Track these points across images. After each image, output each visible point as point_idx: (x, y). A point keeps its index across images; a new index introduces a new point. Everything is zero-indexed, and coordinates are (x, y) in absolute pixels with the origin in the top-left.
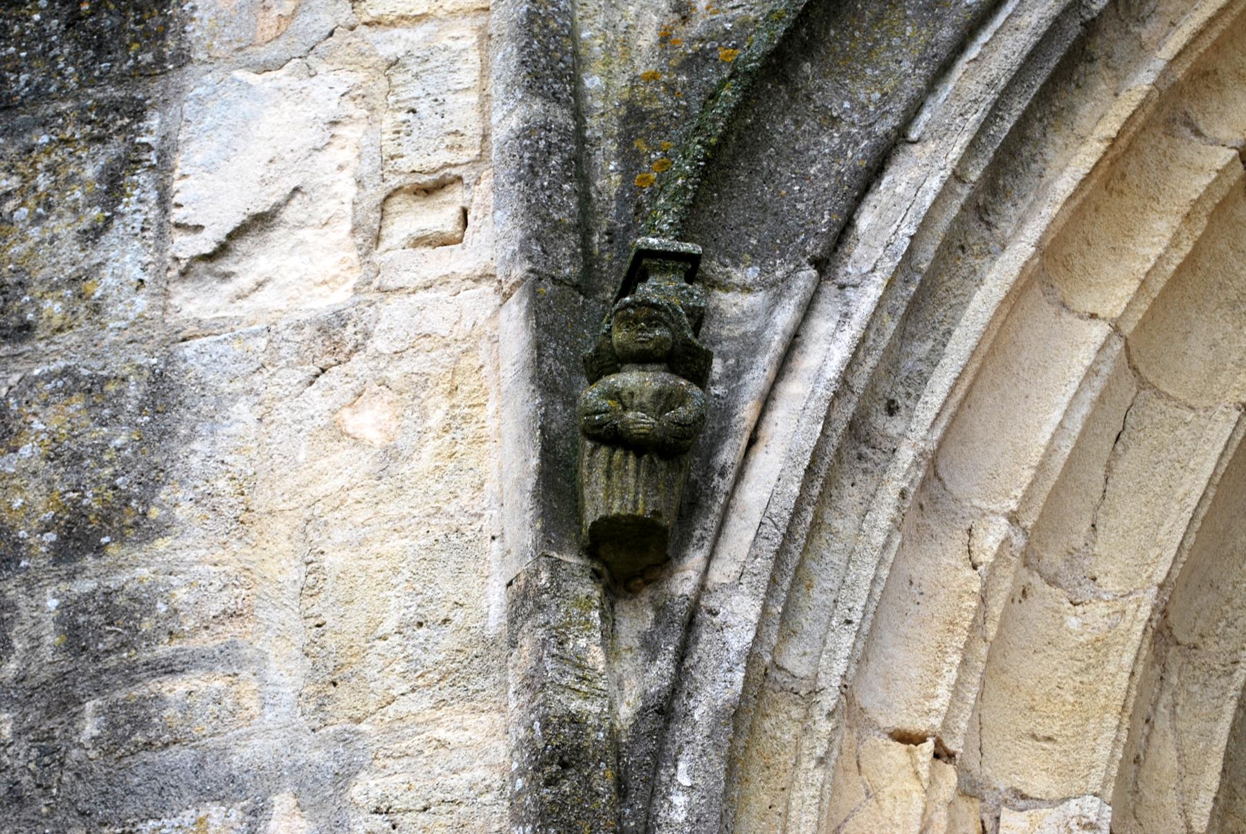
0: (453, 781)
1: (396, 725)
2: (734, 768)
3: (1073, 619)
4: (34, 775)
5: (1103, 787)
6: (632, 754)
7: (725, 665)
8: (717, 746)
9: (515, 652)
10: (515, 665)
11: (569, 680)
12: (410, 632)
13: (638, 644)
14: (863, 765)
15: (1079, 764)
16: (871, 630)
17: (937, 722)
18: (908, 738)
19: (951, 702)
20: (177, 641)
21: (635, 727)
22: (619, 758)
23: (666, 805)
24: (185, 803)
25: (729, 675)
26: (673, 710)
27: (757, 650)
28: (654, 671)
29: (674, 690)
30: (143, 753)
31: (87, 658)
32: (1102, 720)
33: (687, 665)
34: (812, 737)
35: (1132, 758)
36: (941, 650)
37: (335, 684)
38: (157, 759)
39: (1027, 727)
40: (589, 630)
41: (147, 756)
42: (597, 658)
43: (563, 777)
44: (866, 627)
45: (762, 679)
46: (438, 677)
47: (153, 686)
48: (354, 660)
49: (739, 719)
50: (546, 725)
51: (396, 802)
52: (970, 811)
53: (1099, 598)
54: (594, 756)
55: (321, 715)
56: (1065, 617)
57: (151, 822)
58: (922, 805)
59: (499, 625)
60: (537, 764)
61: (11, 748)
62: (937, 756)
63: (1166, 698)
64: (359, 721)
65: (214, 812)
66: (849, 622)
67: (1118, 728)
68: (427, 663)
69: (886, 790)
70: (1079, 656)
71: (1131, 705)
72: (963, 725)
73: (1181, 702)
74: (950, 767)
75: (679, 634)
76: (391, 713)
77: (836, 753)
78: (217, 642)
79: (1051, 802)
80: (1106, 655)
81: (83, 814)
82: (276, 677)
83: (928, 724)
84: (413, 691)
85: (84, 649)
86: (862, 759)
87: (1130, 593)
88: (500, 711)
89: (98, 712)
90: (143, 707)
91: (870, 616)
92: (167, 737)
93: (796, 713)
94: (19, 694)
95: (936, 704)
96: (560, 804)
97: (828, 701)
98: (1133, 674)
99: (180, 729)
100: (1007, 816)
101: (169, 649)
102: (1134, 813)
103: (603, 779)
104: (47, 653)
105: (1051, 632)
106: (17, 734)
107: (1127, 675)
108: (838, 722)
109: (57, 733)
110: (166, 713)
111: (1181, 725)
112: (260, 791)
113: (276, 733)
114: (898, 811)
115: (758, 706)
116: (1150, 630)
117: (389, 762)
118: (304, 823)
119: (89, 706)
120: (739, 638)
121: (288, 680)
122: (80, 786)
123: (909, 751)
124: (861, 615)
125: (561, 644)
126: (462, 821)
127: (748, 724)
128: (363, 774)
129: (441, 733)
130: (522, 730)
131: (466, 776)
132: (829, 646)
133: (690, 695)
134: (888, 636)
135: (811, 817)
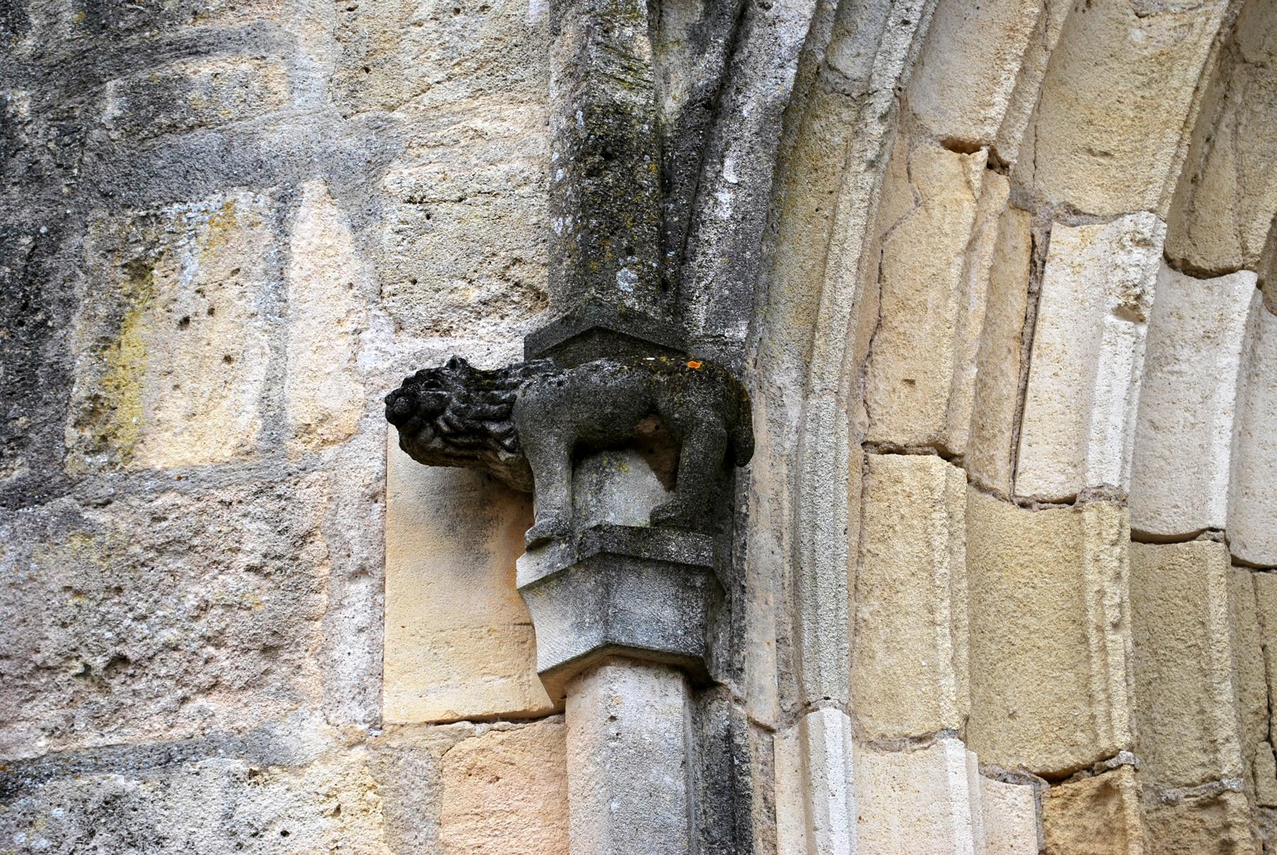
0: (491, 172)
1: (431, 114)
2: (783, 168)
3: (1138, 32)
4: (54, 155)
5: (1160, 203)
6: (677, 148)
7: (777, 61)
8: (766, 144)
9: (558, 40)
10: (558, 54)
11: (613, 69)
12: (446, 18)
13: (686, 37)
14: (913, 172)
15: (1135, 180)
16: (928, 33)
17: (992, 130)
18: (961, 147)
19: (1008, 110)
20: (202, 21)
21: (681, 121)
22: (663, 153)
23: (711, 202)
24: (211, 187)
25: (780, 71)
26: (721, 105)
27: (810, 47)
28: (702, 64)
29: (723, 85)
30: (167, 136)
31: (108, 37)
32: (1163, 135)
33: (737, 59)
34: (863, 139)
35: (1190, 176)
36: (1000, 57)
37: (367, 70)
38: (182, 142)
39: (1084, 142)
40: (636, 19)
41: (172, 139)
42: (643, 47)
43: (606, 168)
44: (924, 29)
45: (814, 77)
46: (475, 66)
47: (176, 67)
48: (387, 46)
49: (790, 116)
50: (589, 114)
51: (431, 192)
52: (1020, 224)
53: (1166, 11)
54: (638, 148)
55: (353, 101)
56: (1130, 29)
57: (176, 206)
58: (972, 215)
59: (540, 14)
60: (579, 154)
61: (30, 127)
62: (990, 166)
63: (1229, 117)
64: (392, 109)
65: (242, 197)
66: (906, 23)
67: (1179, 144)
68: (464, 51)
69: (936, 198)
70: (1142, 70)
71: (1193, 121)
72: (1019, 135)
73: (1244, 122)
74: (1003, 178)
75: (729, 26)
76: (426, 101)
77: (887, 157)
78: (243, 23)
79: (1104, 218)
80: (1170, 70)
81: (105, 195)
82: (305, 62)
83: (983, 132)
84: (449, 79)
85: (104, 27)
86: (913, 167)
87: (1200, 6)
88: (539, 102)
89: (120, 92)
90: (167, 88)
91: (929, 17)
92: (192, 120)
93: (847, 115)
94: (39, 71)
95: (992, 112)
96: (603, 195)
97: (881, 103)
98: (1197, 89)
99: (206, 111)
100: (1058, 232)
101: (193, 29)
102: (1189, 233)
103: (647, 172)
104: (65, 30)
105: (1114, 44)
106: (36, 113)
107: (1191, 90)
108: (891, 125)
109: (77, 113)
110: (191, 96)
111: (1242, 145)
112: (289, 177)
113: (306, 118)
114: (947, 220)
115: (808, 105)
116: (1218, 44)
117: (423, 151)
118: (334, 211)
119: (110, 86)
120: (792, 34)
121: (318, 64)
122: (102, 168)
123: (961, 160)
124: (919, 16)
125: (606, 32)
126: (499, 213)
127: (797, 123)
128: (396, 162)
129: (478, 123)
130: (564, 120)
131: (504, 167)
132: (885, 47)
133: (738, 91)
134: (945, 40)
135: (859, 221)
